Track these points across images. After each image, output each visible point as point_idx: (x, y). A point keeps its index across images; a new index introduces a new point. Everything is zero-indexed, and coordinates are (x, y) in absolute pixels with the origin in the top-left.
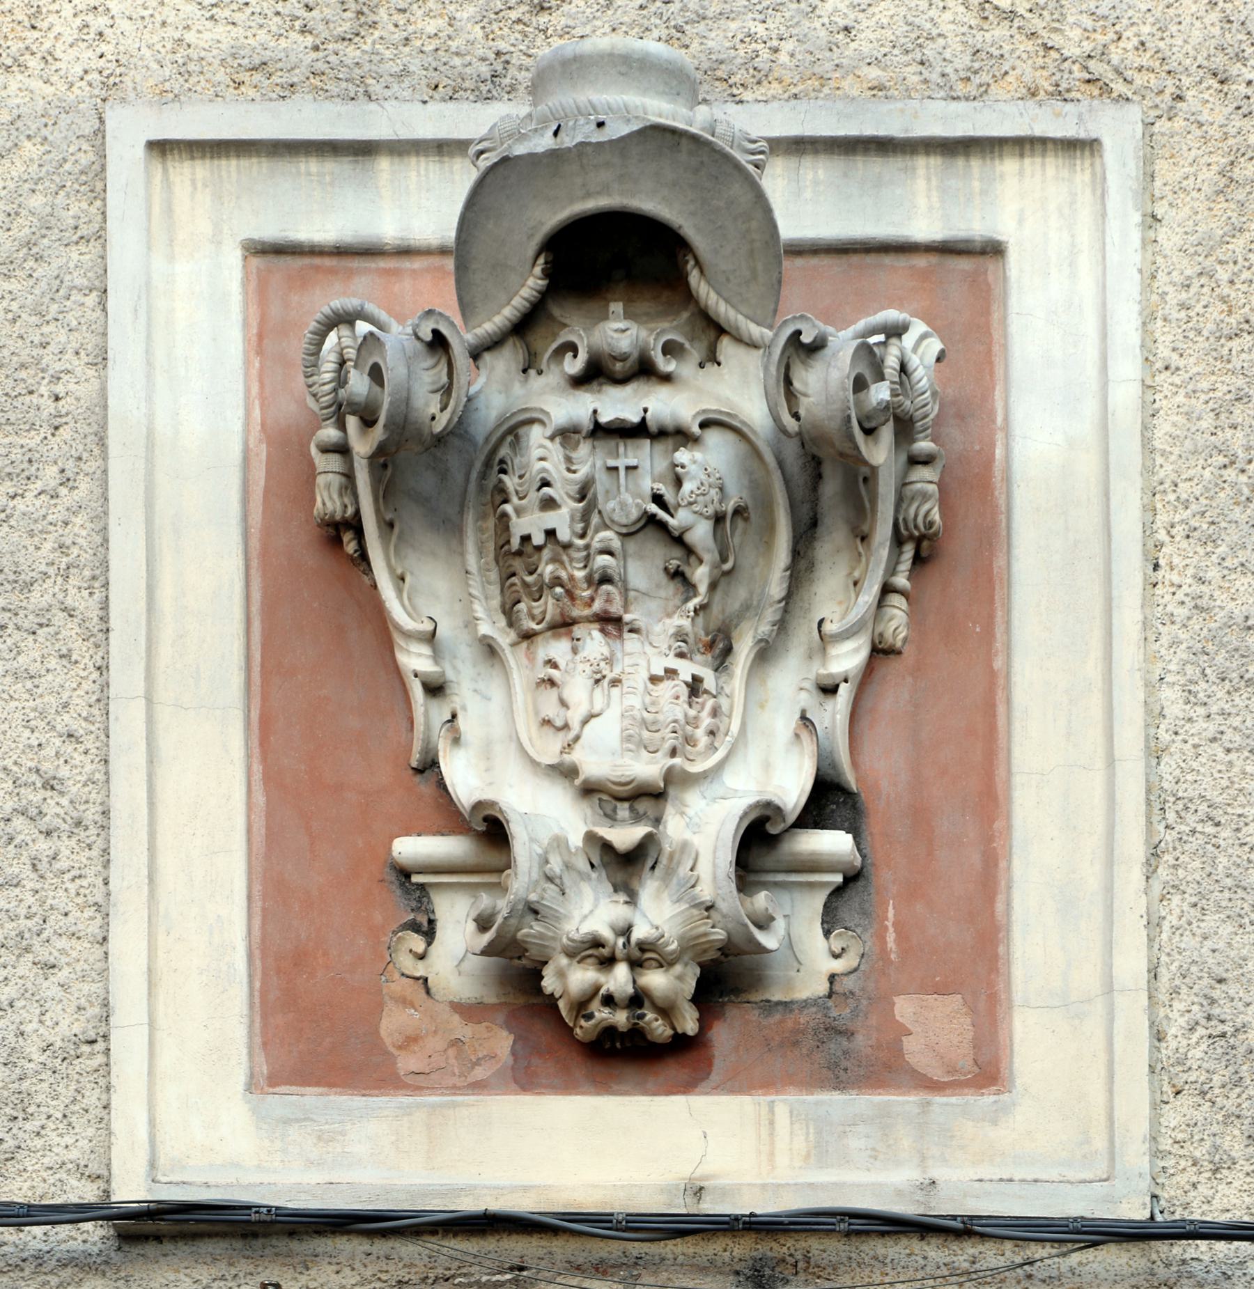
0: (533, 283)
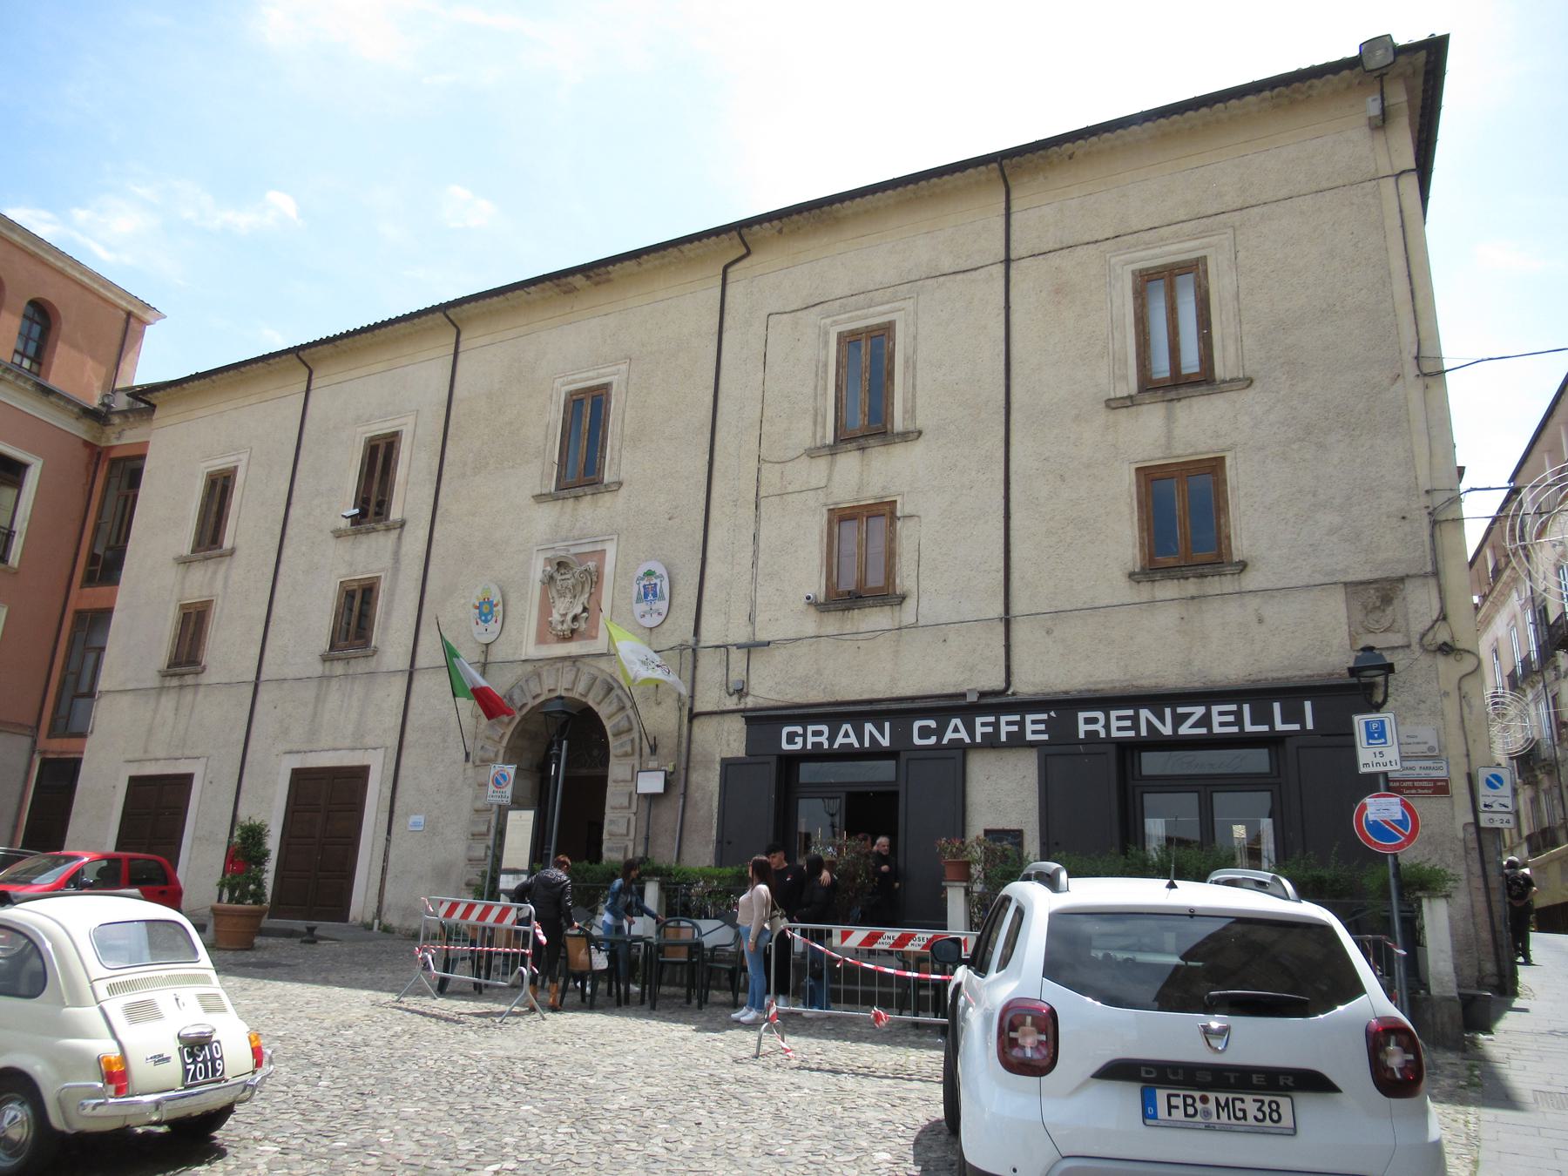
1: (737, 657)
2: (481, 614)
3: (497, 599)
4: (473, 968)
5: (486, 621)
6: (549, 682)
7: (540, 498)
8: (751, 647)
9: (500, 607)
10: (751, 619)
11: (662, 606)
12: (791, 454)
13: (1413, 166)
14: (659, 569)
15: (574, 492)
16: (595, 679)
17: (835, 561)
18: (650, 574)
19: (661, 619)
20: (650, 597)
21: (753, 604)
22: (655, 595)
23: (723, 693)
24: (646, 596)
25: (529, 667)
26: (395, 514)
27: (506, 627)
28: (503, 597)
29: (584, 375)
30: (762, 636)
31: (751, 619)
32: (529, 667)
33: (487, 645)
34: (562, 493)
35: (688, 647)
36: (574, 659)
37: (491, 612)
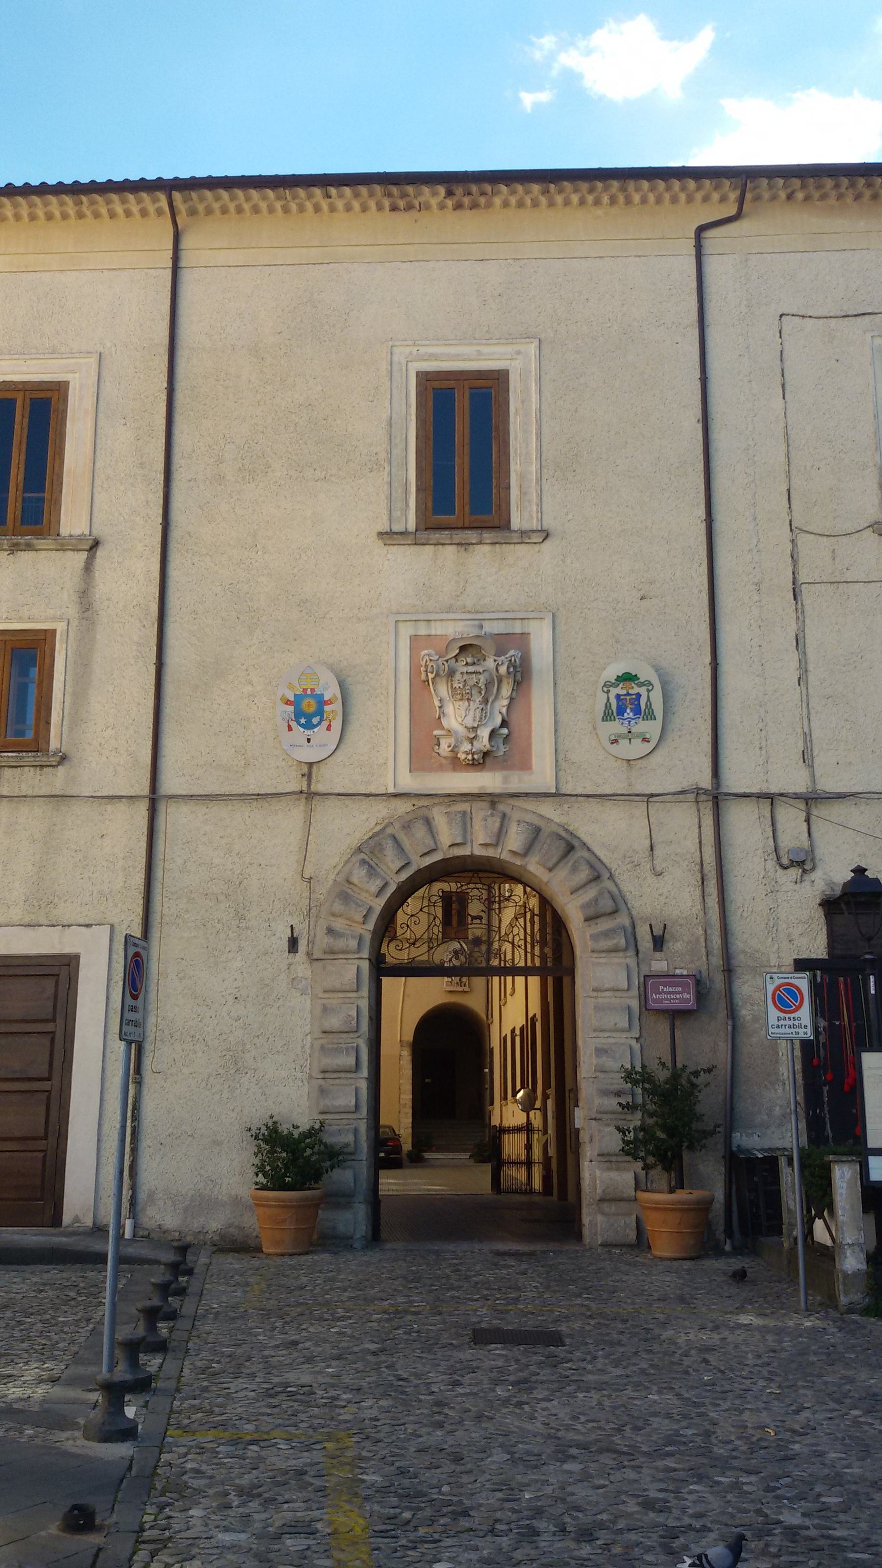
0: (457, 651)
1: (791, 820)
2: (299, 714)
3: (331, 691)
4: (365, 1248)
5: (309, 726)
6: (446, 833)
7: (388, 536)
8: (811, 800)
9: (337, 706)
10: (807, 757)
11: (652, 728)
12: (849, 527)
13: (484, 978)
14: (646, 673)
15: (459, 536)
16: (538, 831)
17: (127, 1149)
18: (627, 678)
19: (649, 747)
20: (629, 714)
21: (807, 737)
22: (637, 711)
23: (771, 864)
24: (621, 711)
25: (403, 807)
26: (72, 520)
27: (348, 739)
28: (342, 685)
29: (452, 350)
30: (829, 784)
31: (807, 757)
32: (403, 807)
33: (311, 765)
34: (423, 536)
35: (706, 792)
36: (492, 799)
37: (320, 712)
